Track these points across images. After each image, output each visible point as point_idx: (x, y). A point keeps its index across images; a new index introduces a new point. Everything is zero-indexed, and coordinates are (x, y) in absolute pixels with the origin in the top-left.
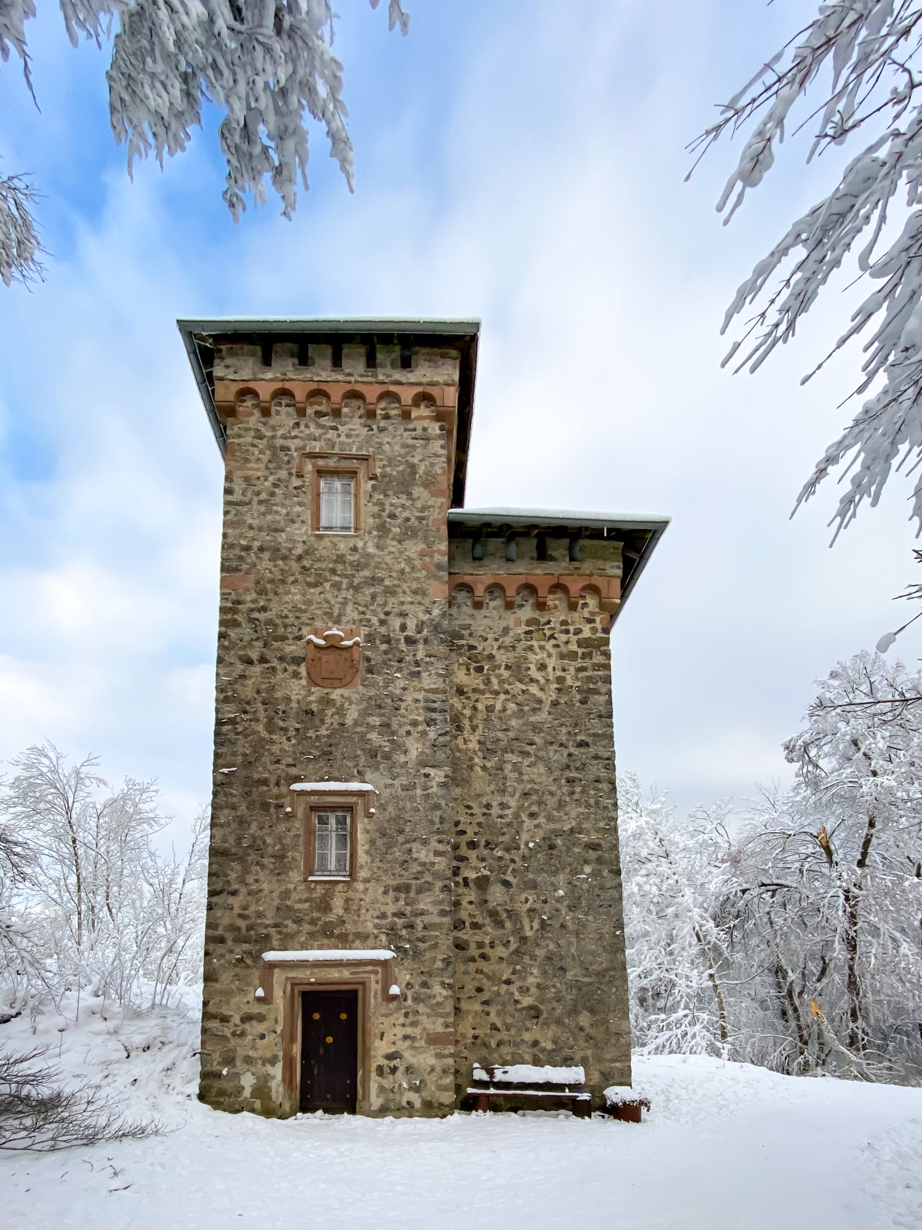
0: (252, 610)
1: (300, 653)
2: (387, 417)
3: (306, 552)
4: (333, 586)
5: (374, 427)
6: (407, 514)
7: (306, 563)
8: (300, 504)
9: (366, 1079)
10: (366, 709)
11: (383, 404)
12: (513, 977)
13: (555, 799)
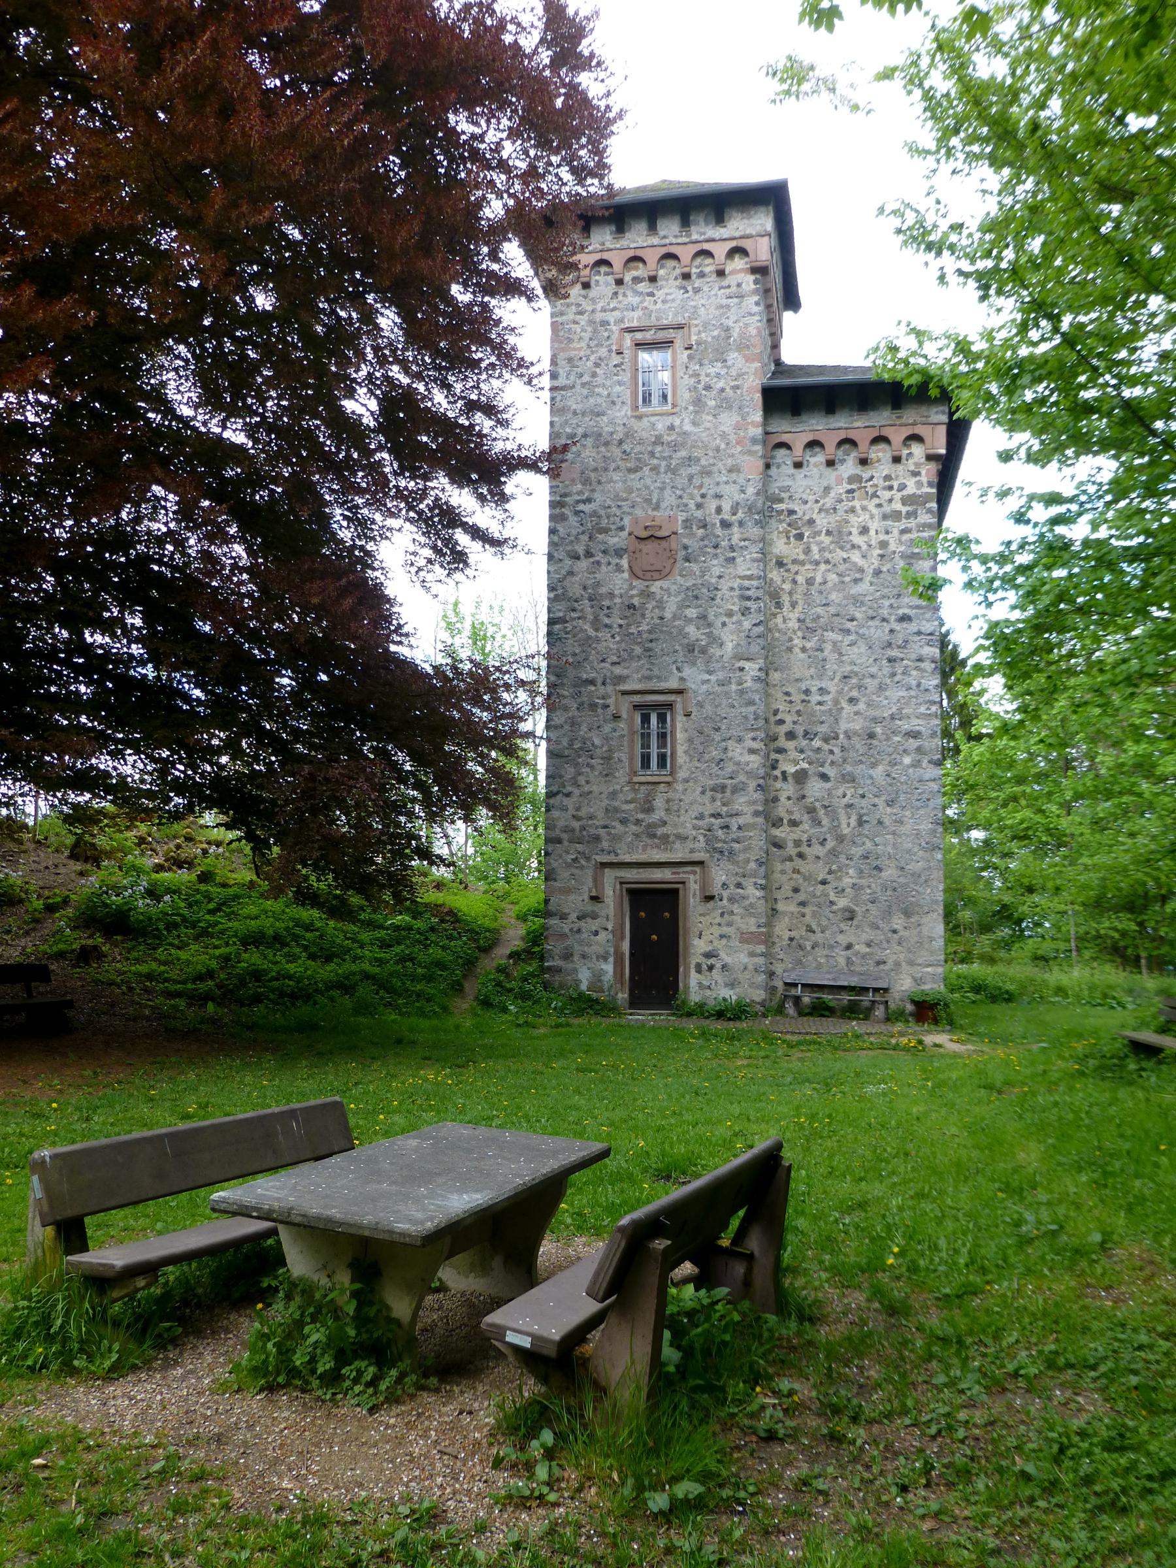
0: (578, 502)
1: (623, 545)
2: (702, 275)
3: (627, 435)
6: (721, 384)
8: (619, 383)
10: (684, 600)
13: (876, 682)
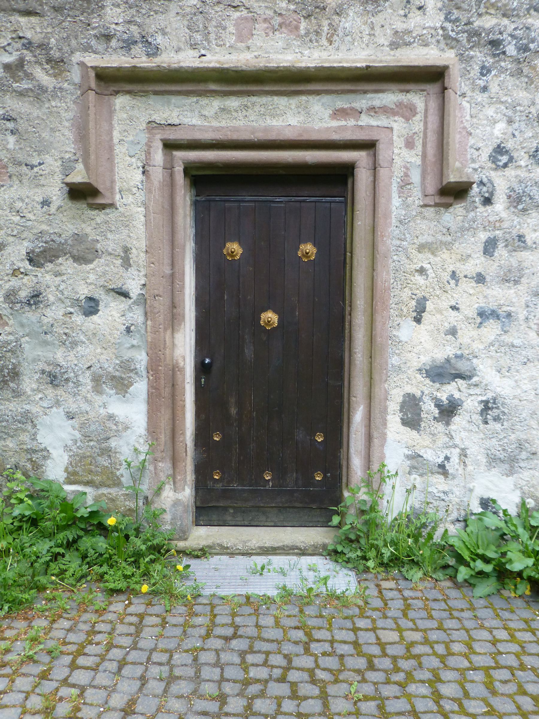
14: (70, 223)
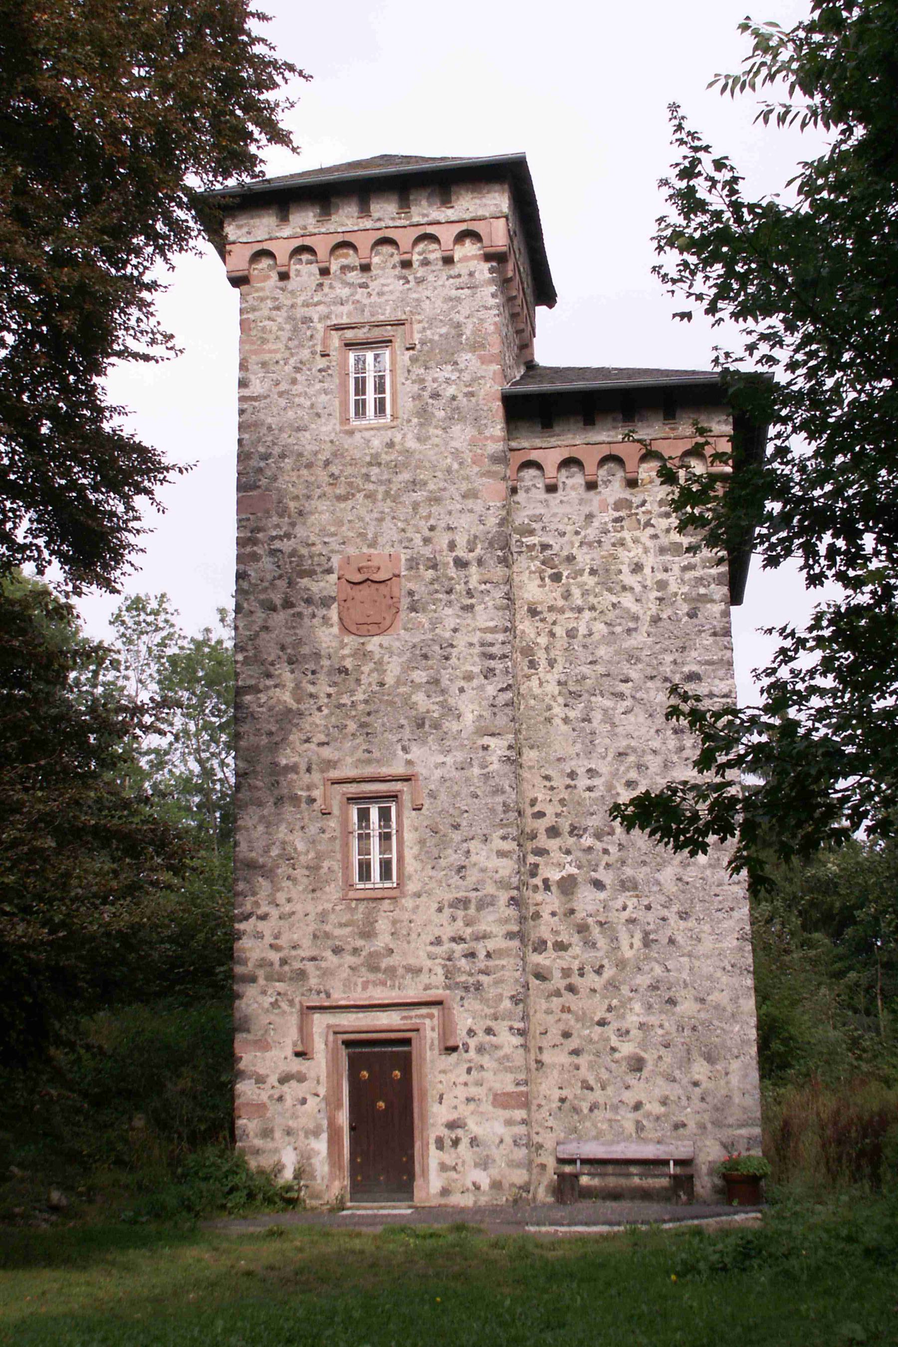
2: (425, 263)
3: (335, 454)
4: (366, 497)
5: (411, 278)
7: (334, 469)
9: (425, 1155)
10: (410, 661)
11: (421, 247)
12: (609, 1016)
13: (659, 760)
14: (297, 1065)
